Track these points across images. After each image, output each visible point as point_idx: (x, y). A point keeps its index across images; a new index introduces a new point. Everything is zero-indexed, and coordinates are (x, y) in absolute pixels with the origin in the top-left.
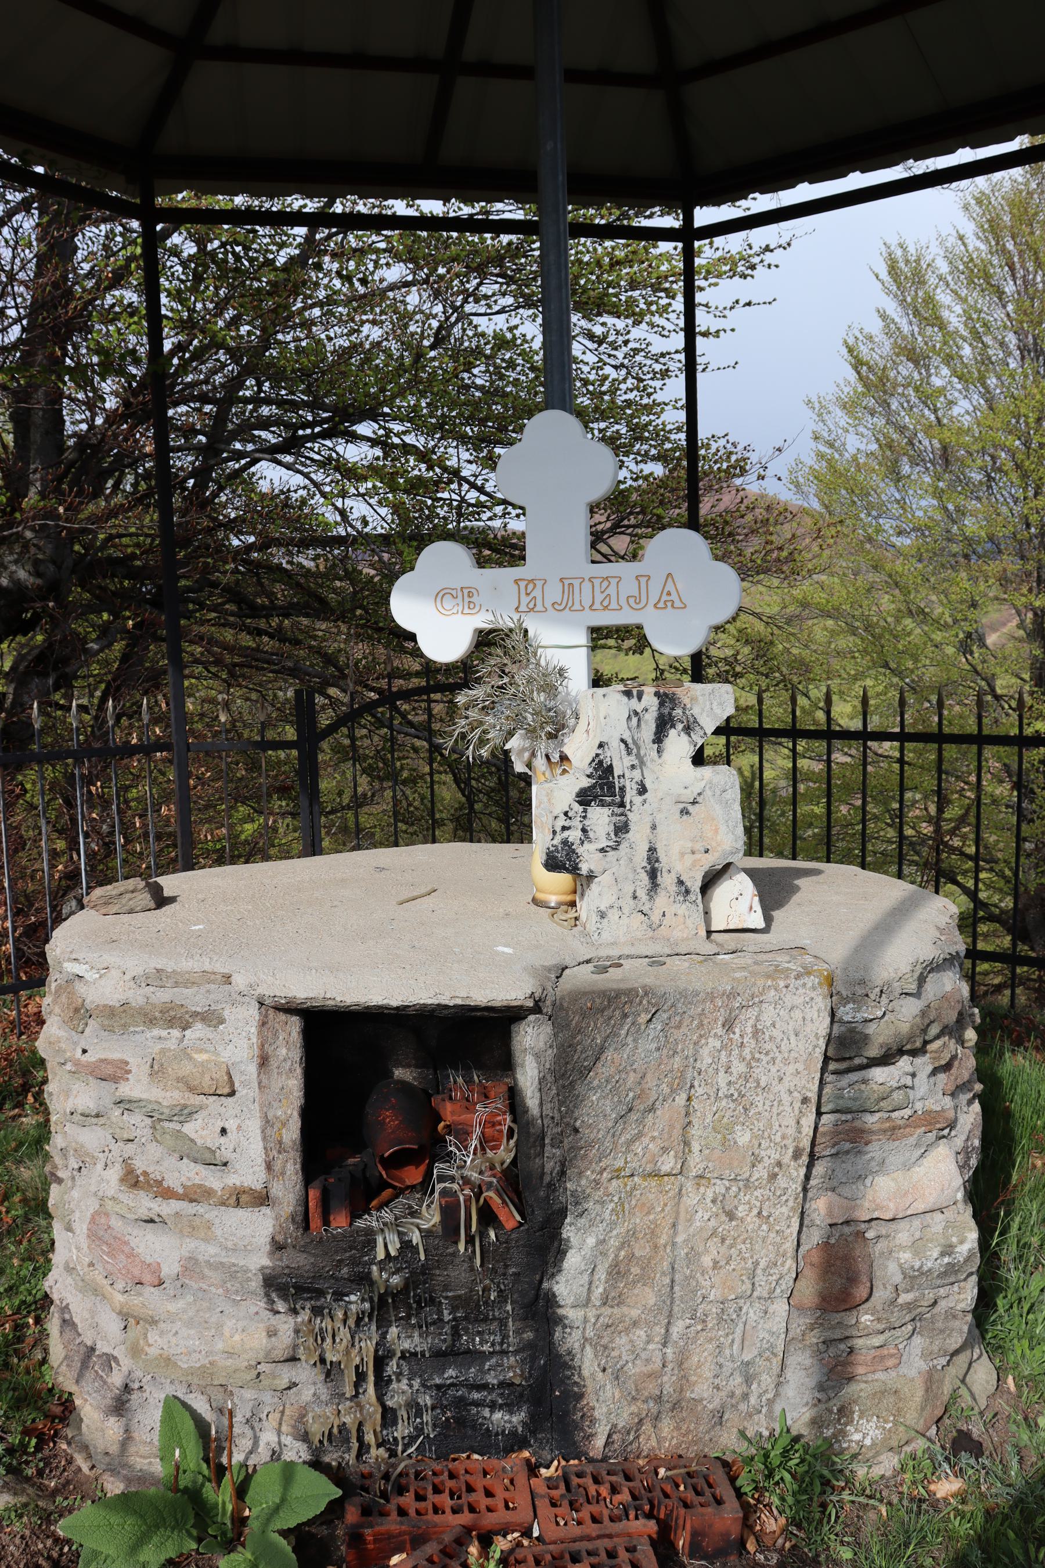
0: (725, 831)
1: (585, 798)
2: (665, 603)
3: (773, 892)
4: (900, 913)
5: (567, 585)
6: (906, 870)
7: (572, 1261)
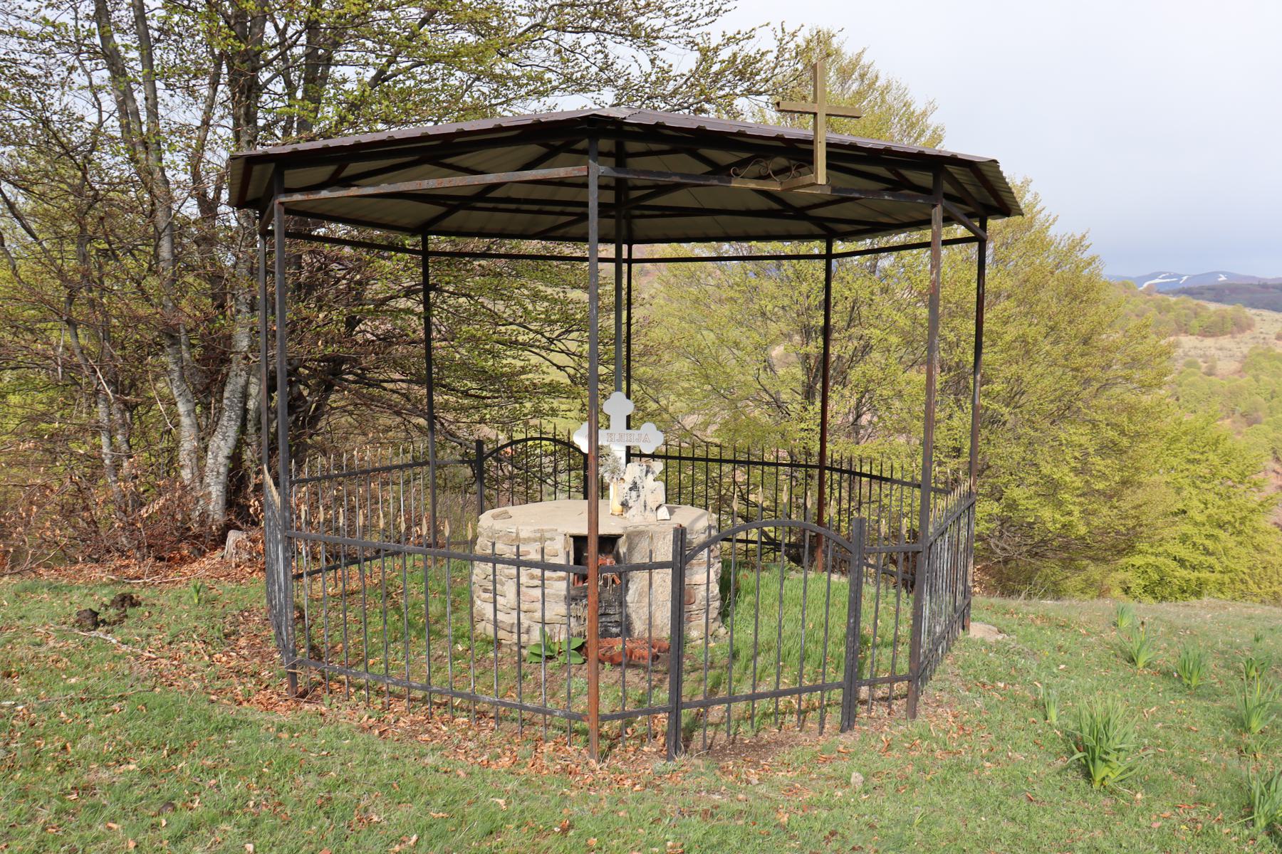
0: (661, 498)
1: (631, 489)
2: (645, 441)
3: (671, 512)
4: (701, 516)
5: (621, 435)
6: (697, 501)
7: (630, 592)
